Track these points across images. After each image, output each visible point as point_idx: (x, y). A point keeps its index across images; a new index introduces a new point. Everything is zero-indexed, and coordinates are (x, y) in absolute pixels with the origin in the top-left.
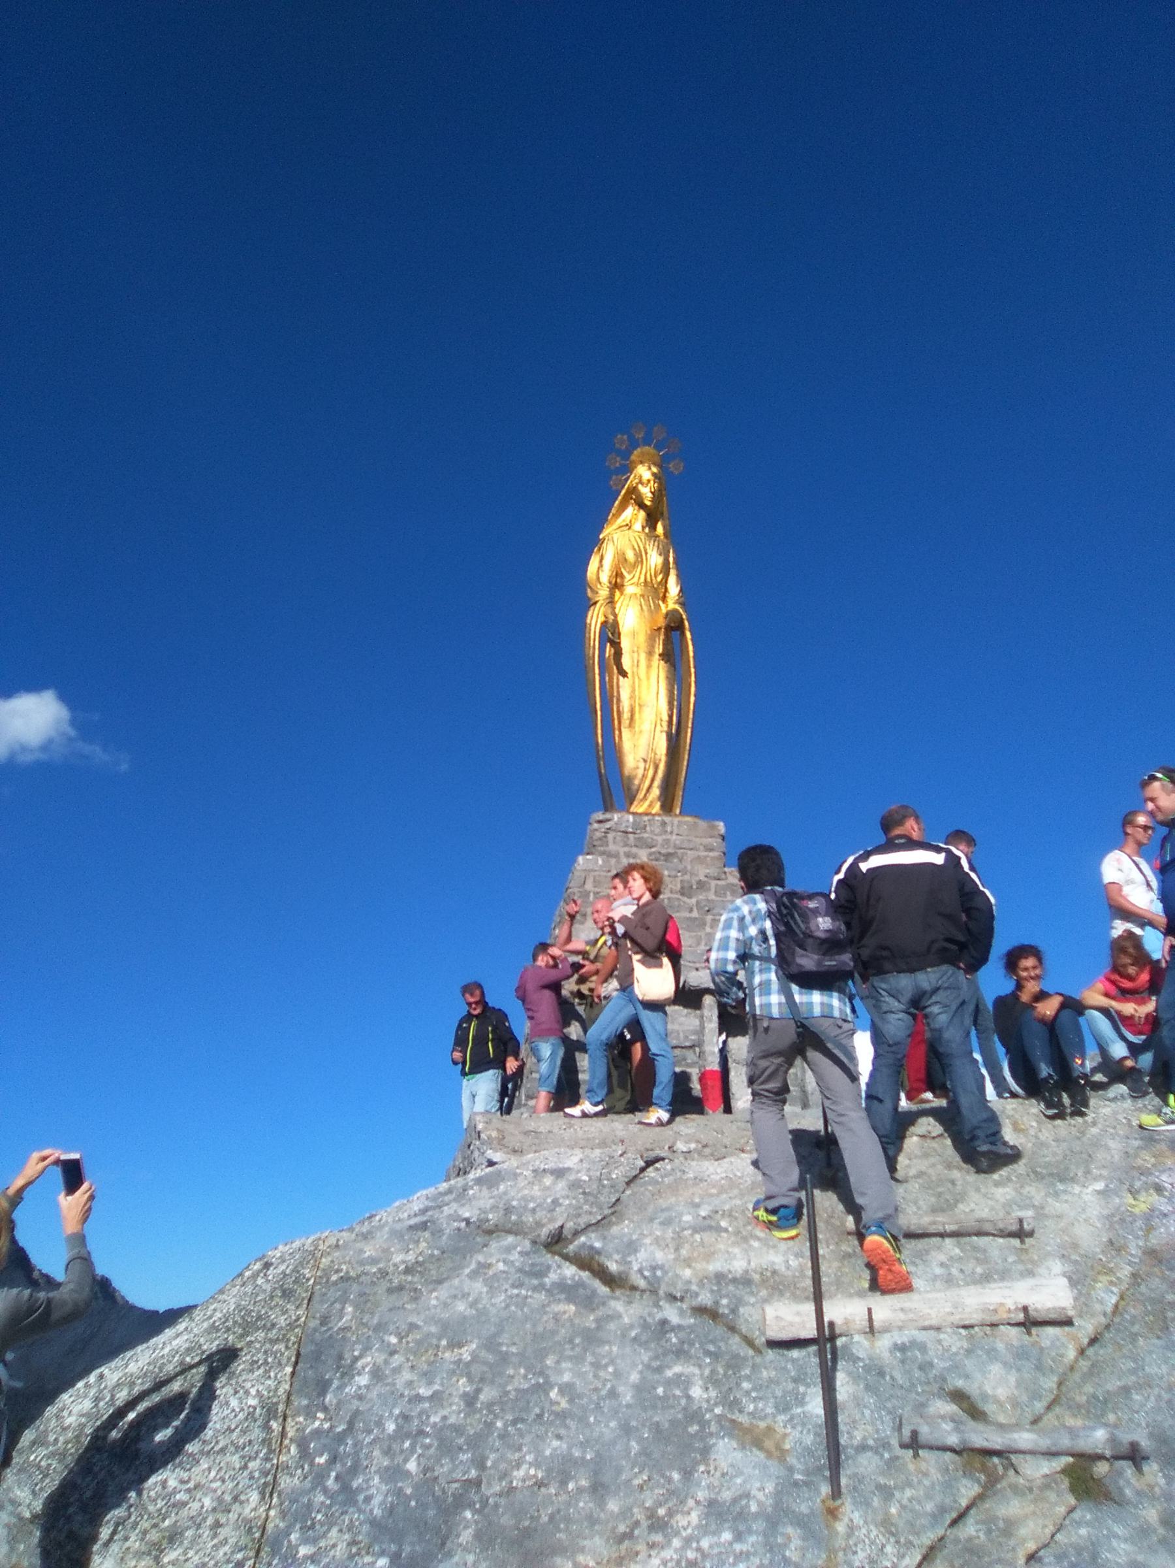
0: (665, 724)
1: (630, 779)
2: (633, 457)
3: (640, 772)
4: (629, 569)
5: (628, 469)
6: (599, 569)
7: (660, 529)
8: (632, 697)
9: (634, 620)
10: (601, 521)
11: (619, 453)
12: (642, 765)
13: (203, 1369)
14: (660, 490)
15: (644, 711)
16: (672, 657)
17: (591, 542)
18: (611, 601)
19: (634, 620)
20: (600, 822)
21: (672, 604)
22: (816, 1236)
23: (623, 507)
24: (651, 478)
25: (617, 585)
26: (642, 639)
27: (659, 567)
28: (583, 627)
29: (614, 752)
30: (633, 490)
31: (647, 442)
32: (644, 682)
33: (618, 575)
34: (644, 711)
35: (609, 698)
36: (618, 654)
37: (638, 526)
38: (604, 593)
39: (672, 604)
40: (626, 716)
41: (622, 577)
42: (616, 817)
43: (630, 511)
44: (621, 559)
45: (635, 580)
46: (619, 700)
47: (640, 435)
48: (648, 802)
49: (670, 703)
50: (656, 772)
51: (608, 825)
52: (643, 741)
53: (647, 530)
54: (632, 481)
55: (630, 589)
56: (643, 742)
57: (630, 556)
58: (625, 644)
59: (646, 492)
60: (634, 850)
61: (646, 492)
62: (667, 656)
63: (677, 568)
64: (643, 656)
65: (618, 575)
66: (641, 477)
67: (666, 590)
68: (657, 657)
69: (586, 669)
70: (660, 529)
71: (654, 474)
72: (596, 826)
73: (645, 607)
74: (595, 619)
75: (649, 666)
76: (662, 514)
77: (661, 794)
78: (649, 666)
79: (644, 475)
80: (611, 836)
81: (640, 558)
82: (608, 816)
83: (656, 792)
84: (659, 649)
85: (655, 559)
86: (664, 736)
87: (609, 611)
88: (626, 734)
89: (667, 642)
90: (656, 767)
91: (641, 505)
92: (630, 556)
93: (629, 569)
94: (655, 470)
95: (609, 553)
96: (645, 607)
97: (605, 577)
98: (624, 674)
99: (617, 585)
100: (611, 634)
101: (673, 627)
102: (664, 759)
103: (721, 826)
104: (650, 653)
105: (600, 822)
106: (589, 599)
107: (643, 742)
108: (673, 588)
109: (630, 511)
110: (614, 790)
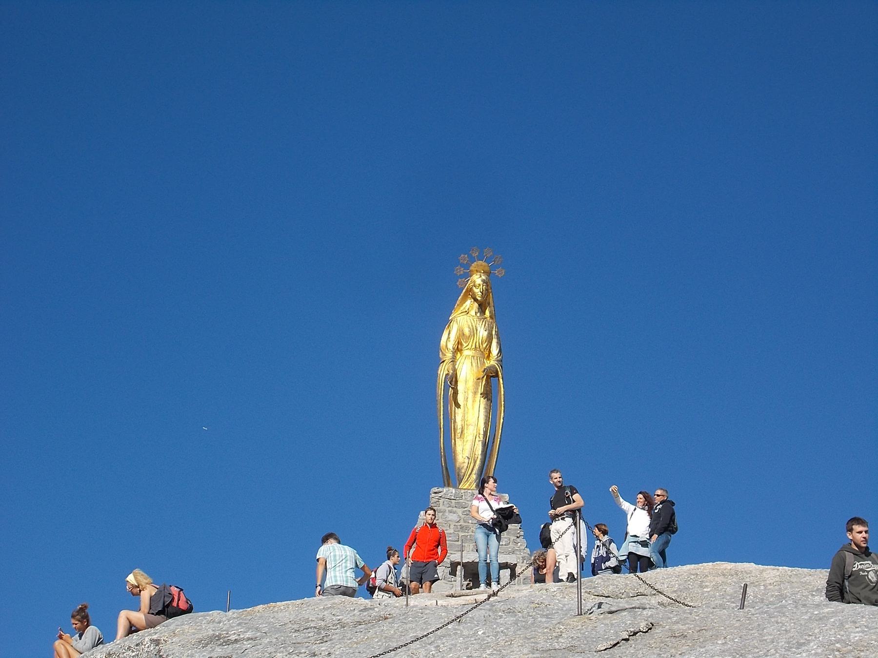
0: (481, 436)
2: (471, 268)
3: (466, 465)
4: (467, 342)
5: (469, 275)
6: (448, 340)
8: (464, 419)
9: (468, 372)
11: (462, 265)
12: (467, 461)
13: (531, 568)
14: (487, 290)
16: (488, 395)
17: (445, 322)
18: (454, 360)
20: (436, 493)
21: (492, 362)
24: (481, 283)
25: (458, 349)
26: (471, 384)
27: (485, 338)
28: (436, 375)
29: (450, 453)
30: (470, 290)
31: (480, 258)
32: (470, 411)
35: (449, 419)
36: (456, 393)
37: (473, 313)
38: (449, 355)
39: (492, 362)
40: (459, 431)
41: (462, 345)
42: (445, 490)
43: (469, 302)
44: (461, 334)
45: (469, 347)
46: (455, 422)
47: (475, 254)
48: (470, 483)
49: (486, 424)
50: (474, 465)
51: (440, 495)
52: (468, 447)
53: (478, 314)
55: (466, 353)
56: (467, 448)
57: (467, 331)
58: (461, 387)
59: (477, 291)
60: (455, 509)
63: (498, 338)
64: (471, 395)
66: (475, 282)
67: (490, 352)
68: (479, 395)
69: (435, 402)
71: (483, 281)
72: (433, 495)
73: (474, 364)
74: (443, 371)
76: (489, 304)
77: (477, 478)
78: (474, 401)
79: (478, 279)
80: (441, 501)
82: (440, 489)
83: (474, 476)
84: (481, 390)
86: (480, 443)
87: (451, 367)
88: (459, 442)
89: (488, 384)
90: (475, 462)
91: (475, 300)
93: (467, 342)
94: (483, 277)
95: (454, 328)
96: (474, 364)
98: (458, 406)
99: (458, 349)
100: (453, 380)
101: (491, 375)
102: (480, 457)
104: (475, 393)
105: (436, 493)
106: (440, 359)
107: (467, 448)
108: (495, 350)
109: (469, 302)
110: (449, 475)
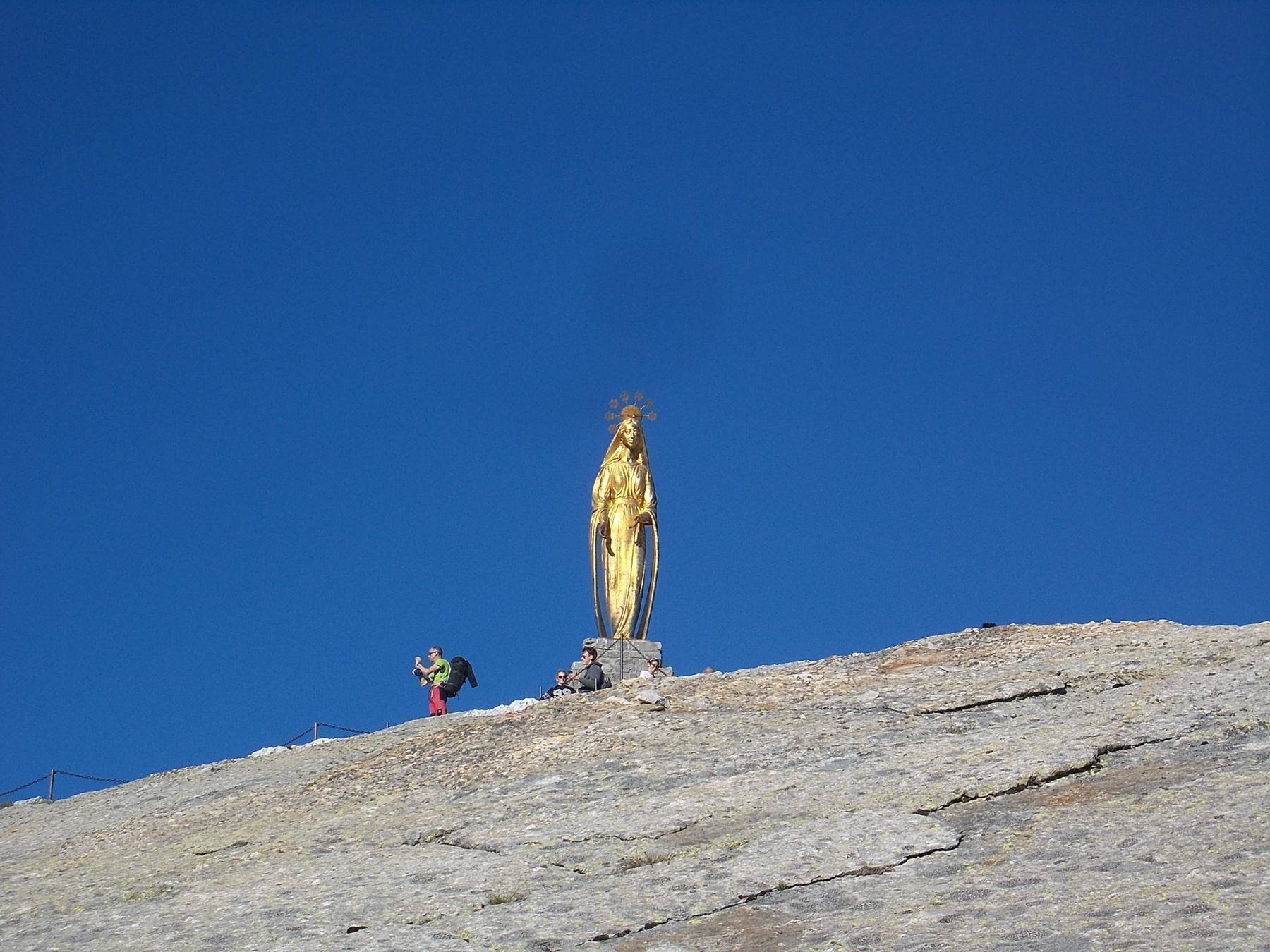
1: (614, 619)
4: (618, 485)
6: (600, 488)
7: (640, 459)
8: (616, 569)
9: (620, 520)
10: (601, 456)
15: (623, 569)
17: (596, 470)
18: (606, 509)
19: (620, 520)
22: (638, 603)
23: (615, 447)
25: (610, 498)
26: (623, 533)
29: (603, 604)
33: (611, 491)
34: (623, 569)
37: (625, 459)
38: (601, 504)
39: (646, 509)
40: (612, 581)
43: (620, 449)
44: (613, 479)
52: (621, 596)
54: (620, 430)
55: (619, 501)
56: (621, 598)
57: (618, 479)
58: (613, 536)
59: (629, 437)
61: (629, 437)
62: (640, 543)
64: (623, 544)
65: (611, 491)
69: (589, 553)
70: (640, 459)
74: (595, 520)
75: (627, 550)
78: (627, 550)
81: (626, 479)
83: (628, 626)
85: (635, 480)
88: (612, 592)
91: (627, 446)
92: (618, 479)
93: (618, 485)
95: (606, 476)
97: (602, 495)
98: (612, 555)
99: (610, 498)
100: (605, 530)
103: (659, 645)
104: (628, 542)
107: (621, 598)
108: (648, 497)
110: (604, 627)
